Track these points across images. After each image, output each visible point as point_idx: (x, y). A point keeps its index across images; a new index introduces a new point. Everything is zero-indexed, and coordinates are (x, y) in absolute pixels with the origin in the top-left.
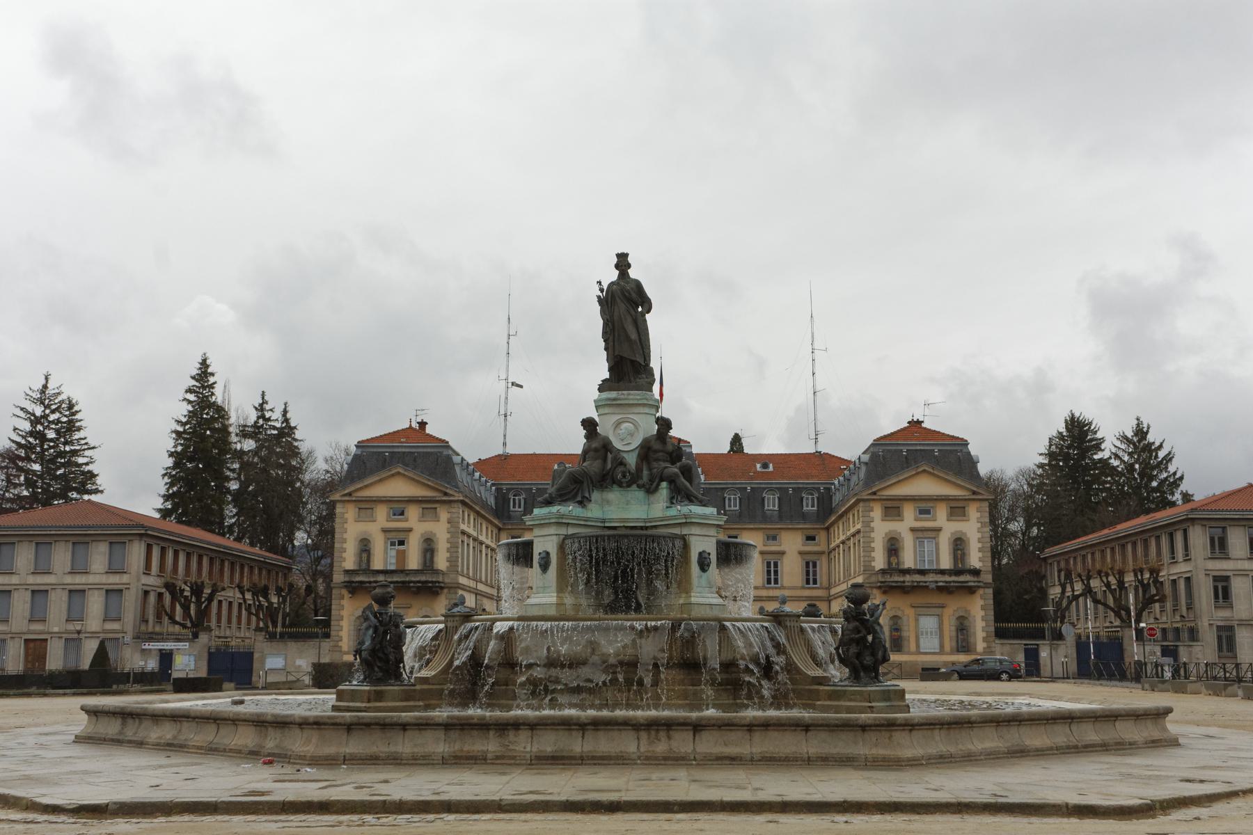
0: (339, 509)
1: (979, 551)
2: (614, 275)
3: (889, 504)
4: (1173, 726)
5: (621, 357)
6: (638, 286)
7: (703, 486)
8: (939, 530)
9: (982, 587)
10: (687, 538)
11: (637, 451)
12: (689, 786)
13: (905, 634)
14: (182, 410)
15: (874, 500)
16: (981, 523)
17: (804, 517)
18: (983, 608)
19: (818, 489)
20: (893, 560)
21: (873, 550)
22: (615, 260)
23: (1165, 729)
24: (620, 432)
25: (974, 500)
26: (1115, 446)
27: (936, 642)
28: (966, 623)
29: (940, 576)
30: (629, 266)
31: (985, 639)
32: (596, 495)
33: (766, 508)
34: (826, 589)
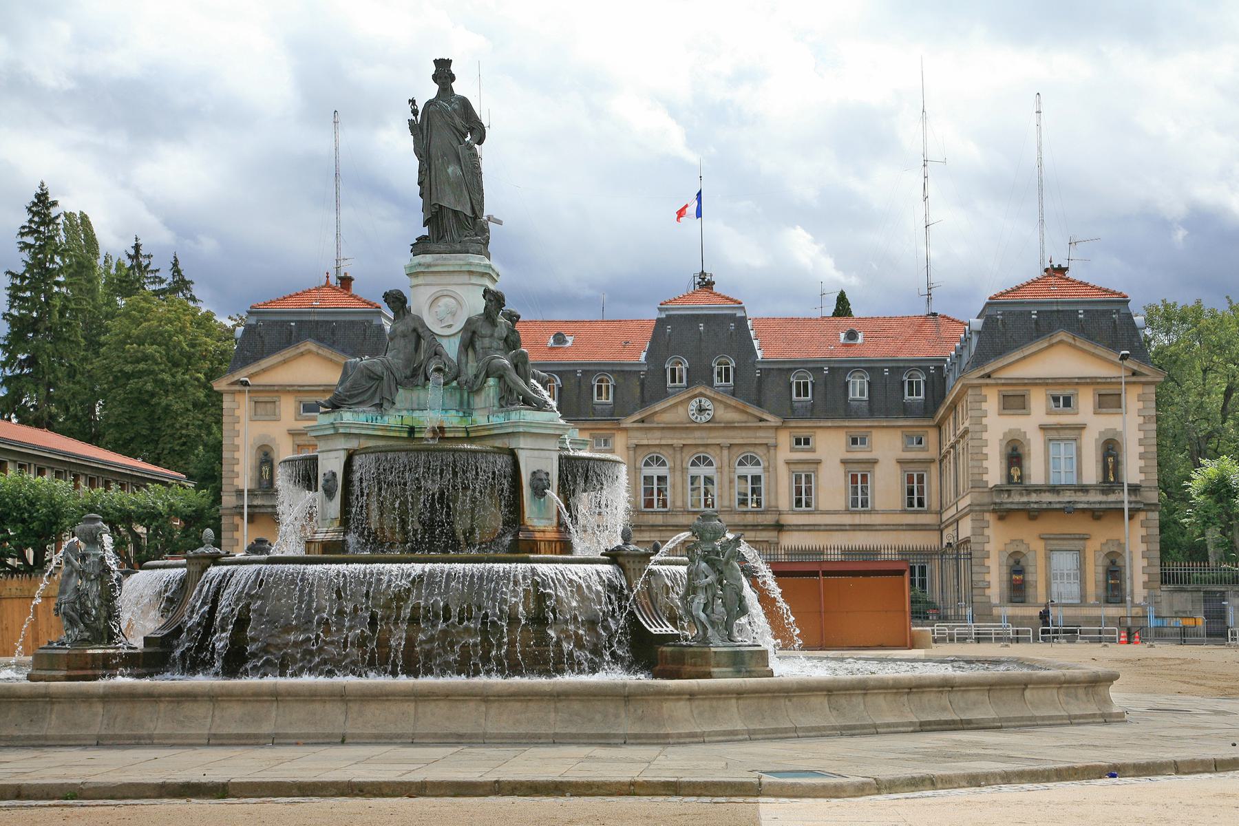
0: (227, 403)
2: (432, 90)
3: (1010, 390)
4: (1118, 696)
5: (441, 206)
6: (465, 104)
7: (760, 366)
8: (1081, 428)
9: (1143, 510)
10: (516, 450)
11: (460, 335)
13: (1030, 578)
14: (19, 261)
15: (987, 385)
17: (907, 411)
18: (1145, 539)
19: (926, 370)
20: (1015, 472)
21: (986, 457)
22: (433, 69)
23: (1107, 701)
24: (438, 309)
25: (1134, 383)
27: (1075, 589)
28: (1119, 562)
29: (1080, 494)
30: (452, 78)
31: (1146, 585)
32: (401, 395)
33: (851, 396)
34: (936, 513)
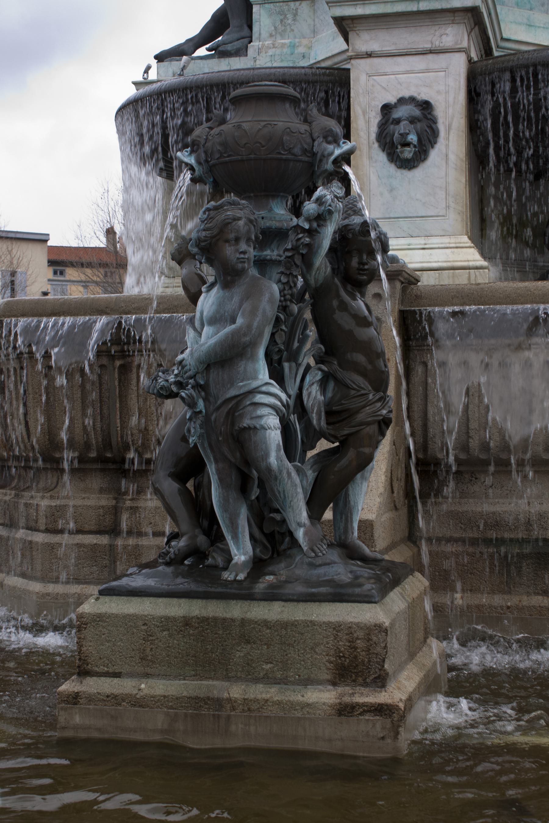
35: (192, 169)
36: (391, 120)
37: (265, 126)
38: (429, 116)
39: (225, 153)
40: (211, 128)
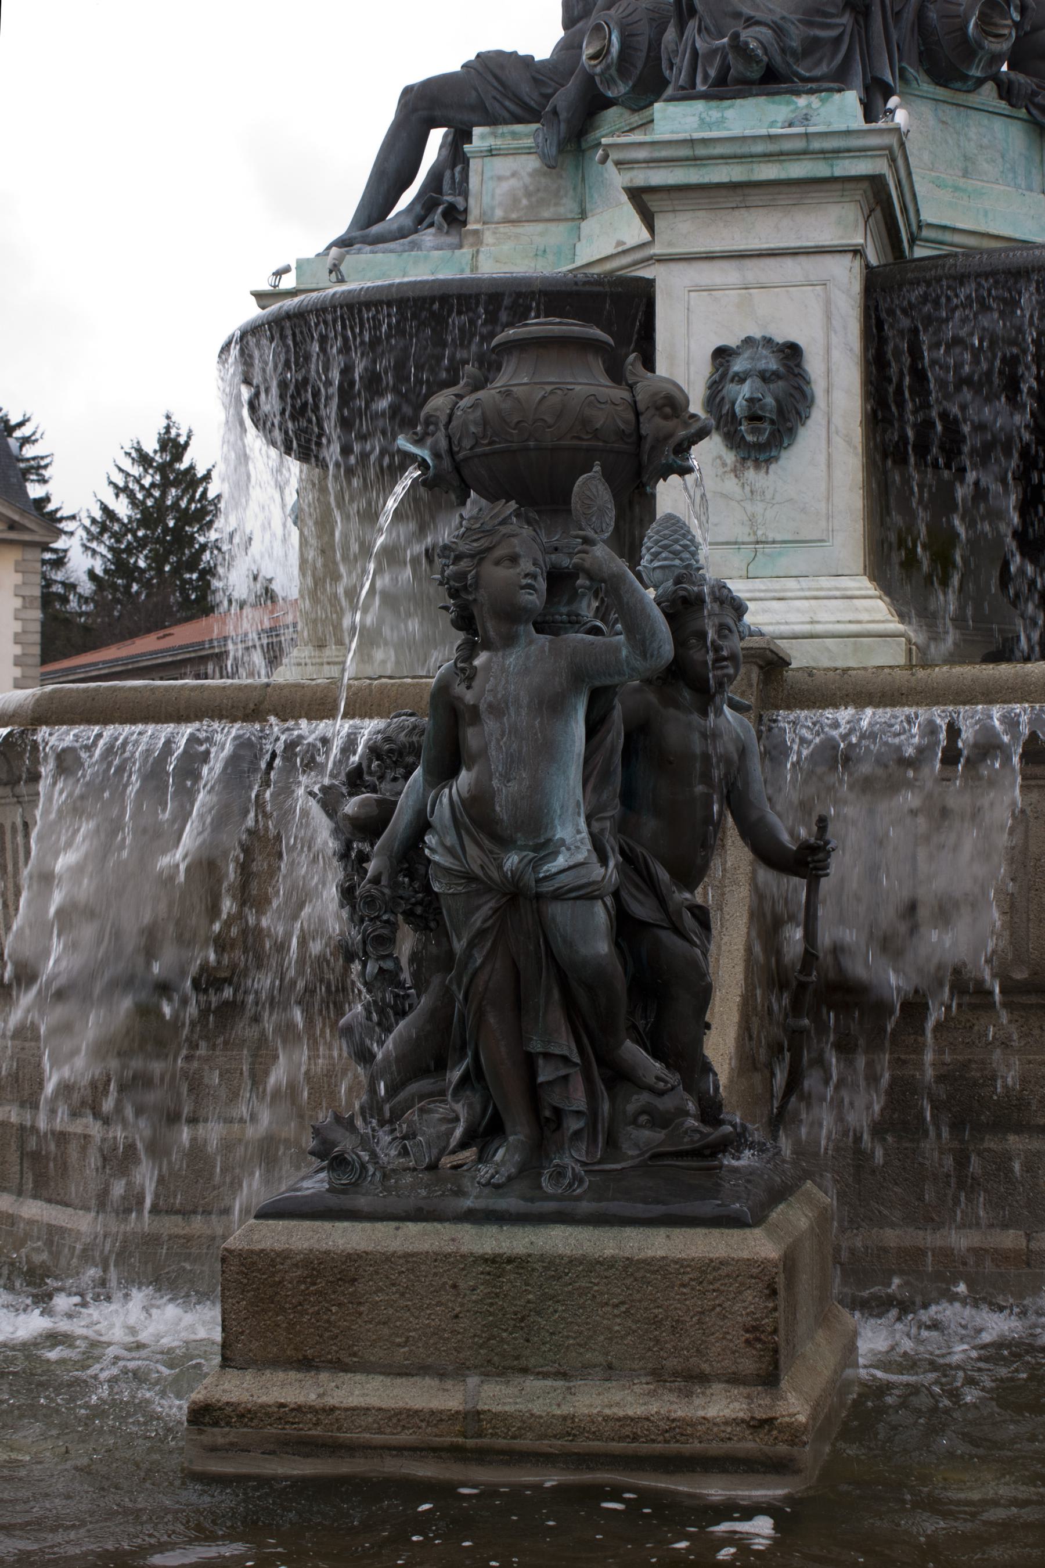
1: (16, 665)
12: (871, 812)
16: (24, 597)
26: (121, 470)
35: (423, 465)
36: (730, 374)
37: (552, 392)
38: (796, 370)
39: (484, 437)
40: (460, 397)
